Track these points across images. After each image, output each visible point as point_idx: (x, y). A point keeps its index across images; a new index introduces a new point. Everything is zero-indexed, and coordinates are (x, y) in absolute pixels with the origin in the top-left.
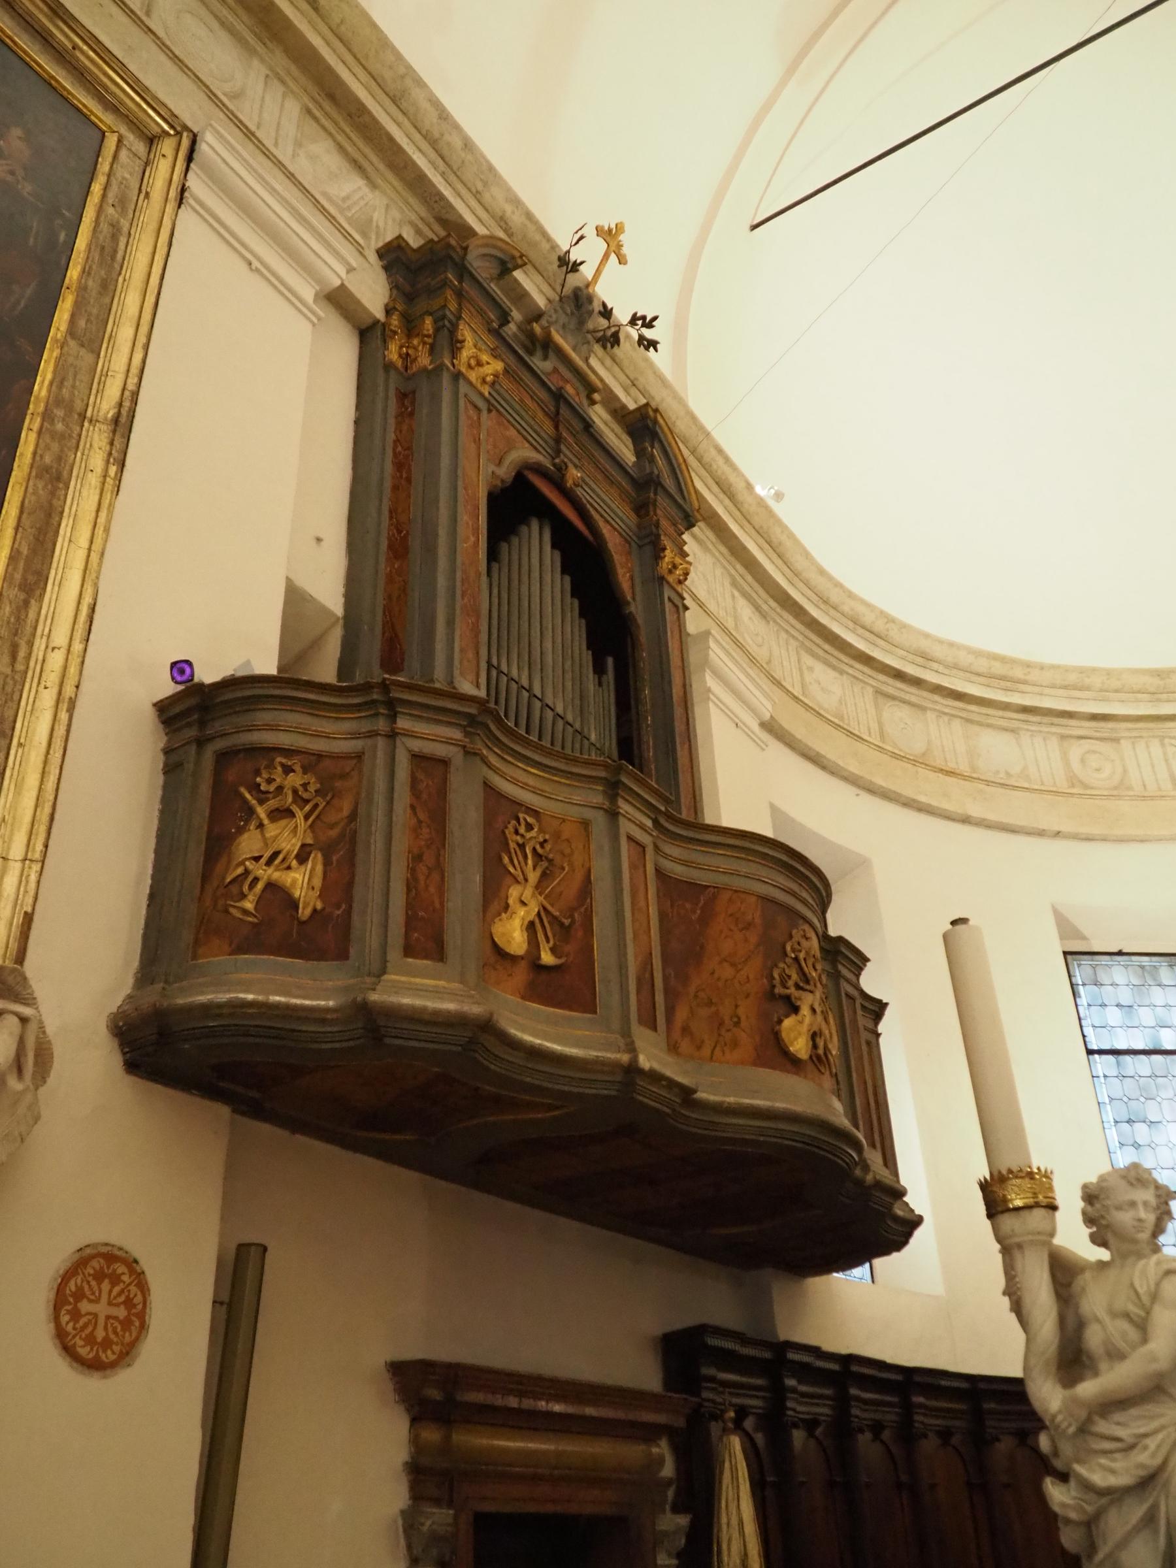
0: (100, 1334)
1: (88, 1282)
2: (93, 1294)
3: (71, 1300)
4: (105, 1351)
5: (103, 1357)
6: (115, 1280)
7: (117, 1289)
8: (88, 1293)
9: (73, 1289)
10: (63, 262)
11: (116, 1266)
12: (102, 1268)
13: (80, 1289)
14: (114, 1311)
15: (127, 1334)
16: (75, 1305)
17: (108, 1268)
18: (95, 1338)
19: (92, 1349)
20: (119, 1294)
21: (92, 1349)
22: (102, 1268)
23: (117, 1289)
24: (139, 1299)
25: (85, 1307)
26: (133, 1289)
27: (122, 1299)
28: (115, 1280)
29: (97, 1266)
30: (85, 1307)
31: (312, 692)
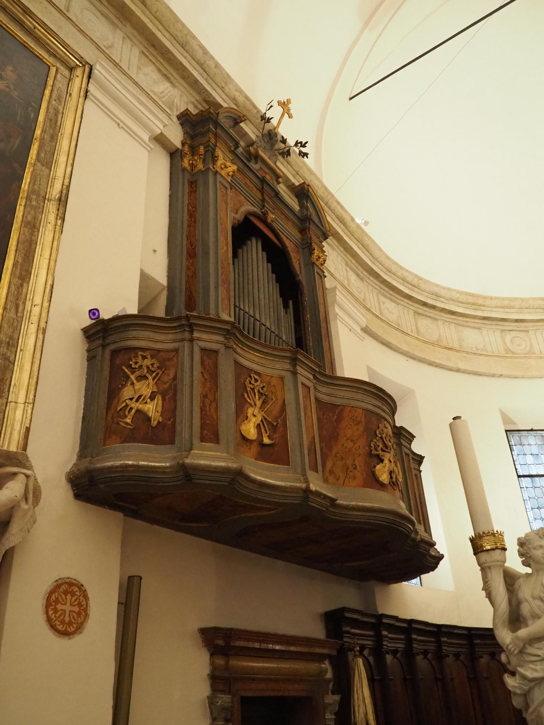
0: (67, 619)
1: (61, 596)
3: (53, 604)
4: (67, 589)
5: (69, 629)
6: (73, 594)
7: (74, 598)
9: (54, 599)
11: (73, 587)
13: (57, 599)
14: (63, 607)
18: (65, 621)
26: (81, 598)
28: (73, 594)
29: (65, 589)
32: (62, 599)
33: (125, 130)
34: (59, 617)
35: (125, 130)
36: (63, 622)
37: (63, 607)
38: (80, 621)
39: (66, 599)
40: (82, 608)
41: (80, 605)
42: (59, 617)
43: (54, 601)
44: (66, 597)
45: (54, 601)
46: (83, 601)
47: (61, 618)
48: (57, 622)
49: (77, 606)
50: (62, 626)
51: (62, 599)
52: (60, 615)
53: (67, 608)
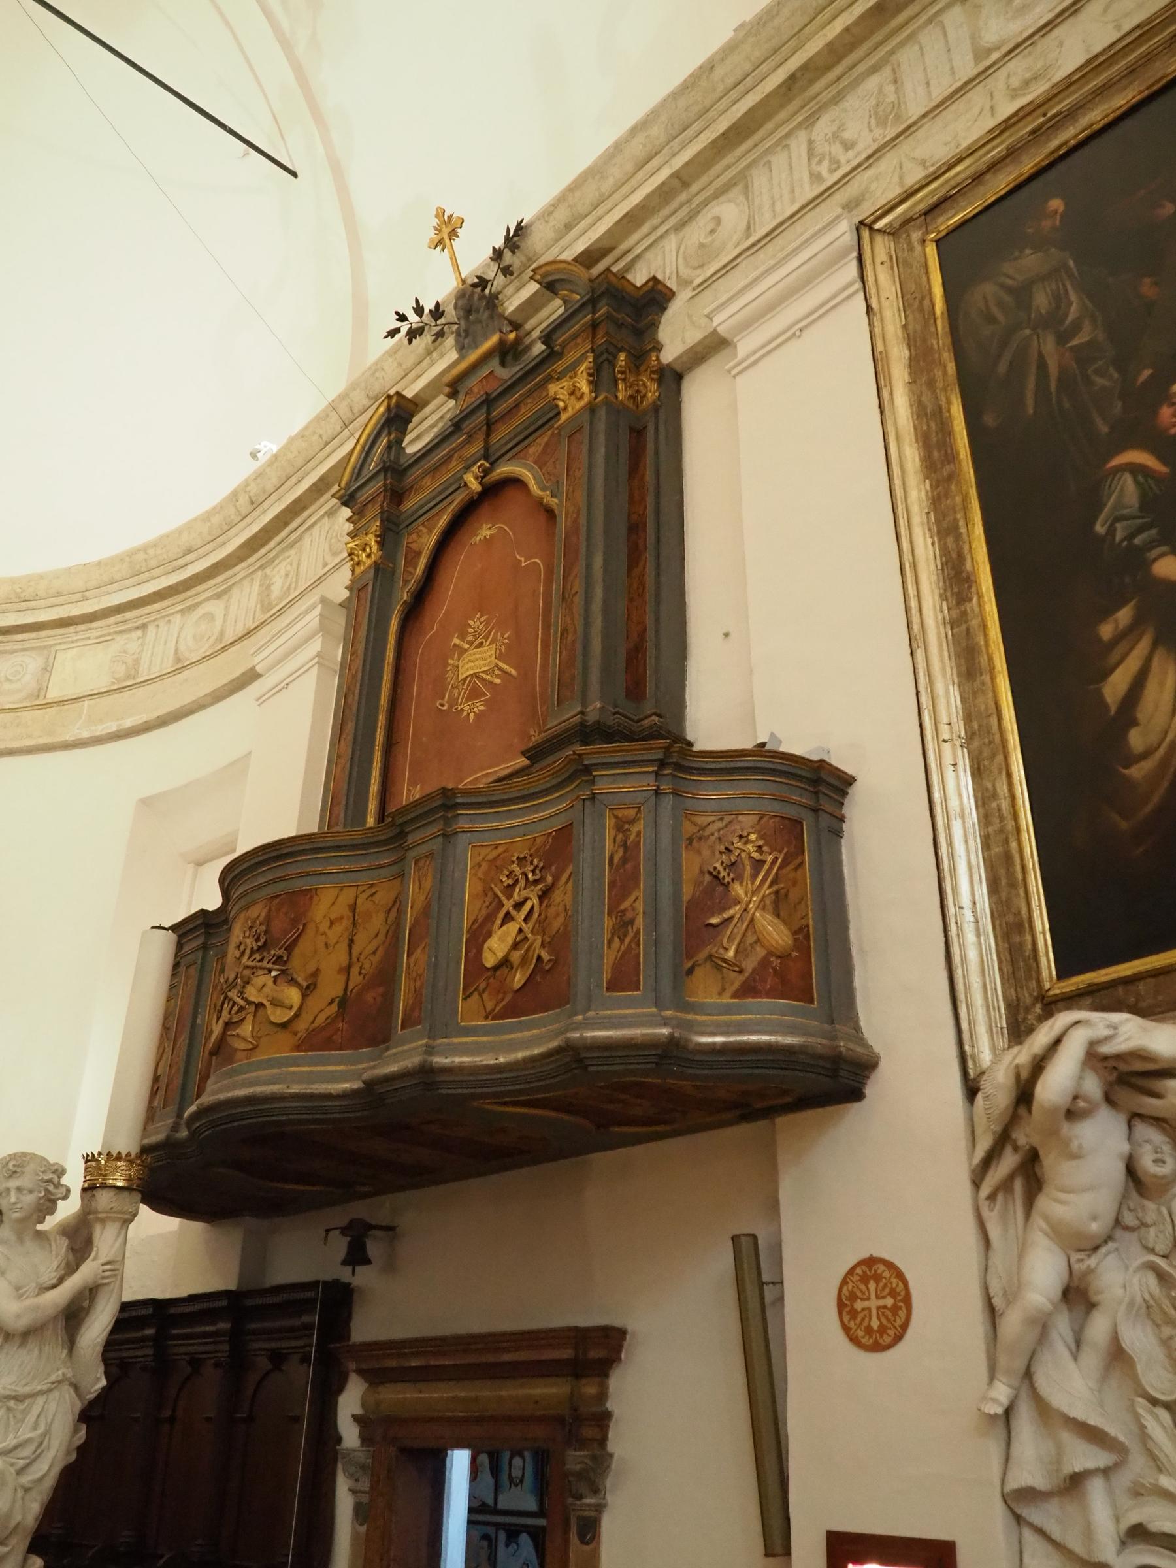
0: (875, 1324)
1: (857, 1287)
2: (863, 1293)
3: (848, 1303)
4: (881, 1336)
5: (881, 1341)
6: (877, 1278)
7: (866, 1323)
8: (859, 1294)
9: (847, 1294)
10: (625, 221)
11: (875, 1267)
12: (864, 1273)
13: (895, 1314)
14: (866, 1304)
15: (897, 1318)
16: (852, 1306)
17: (870, 1271)
18: (872, 1328)
19: (876, 1271)
20: (863, 1320)
21: (876, 1271)
22: (864, 1273)
23: (866, 1323)
24: (846, 1318)
25: (859, 1305)
26: (852, 1324)
27: (887, 1290)
28: (877, 1278)
29: (885, 1336)
30: (859, 1305)
31: (1049, 140)
32: (861, 1291)
33: (806, 326)
34: (861, 1324)
35: (806, 326)
36: (869, 1330)
37: (866, 1304)
38: (898, 1323)
39: (868, 1289)
40: (899, 1298)
41: (854, 1314)
42: (861, 1324)
43: (900, 1308)
44: (881, 1323)
45: (900, 1308)
46: (897, 1285)
47: (881, 1284)
48: (859, 1331)
49: (859, 1309)
50: (879, 1272)
51: (861, 1291)
52: (863, 1320)
53: (873, 1303)
